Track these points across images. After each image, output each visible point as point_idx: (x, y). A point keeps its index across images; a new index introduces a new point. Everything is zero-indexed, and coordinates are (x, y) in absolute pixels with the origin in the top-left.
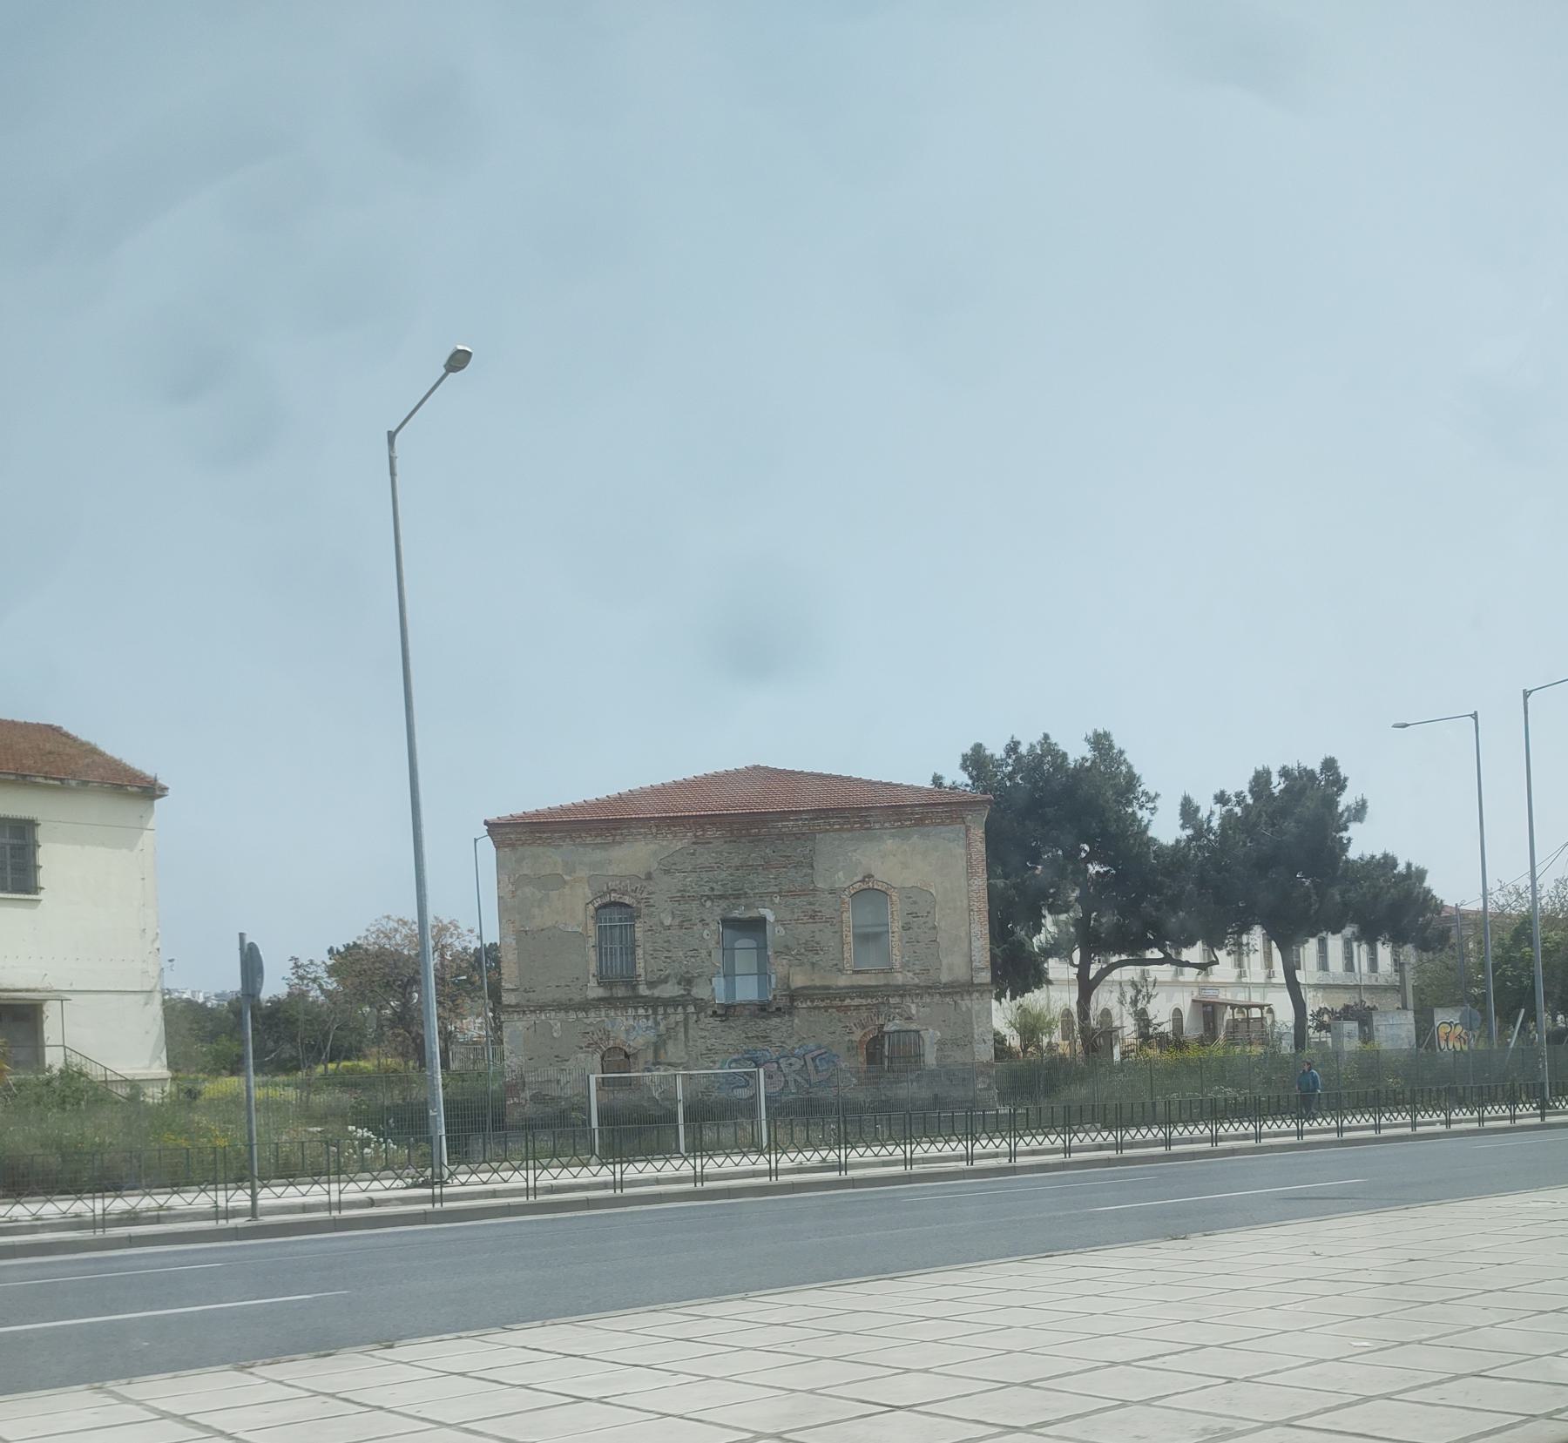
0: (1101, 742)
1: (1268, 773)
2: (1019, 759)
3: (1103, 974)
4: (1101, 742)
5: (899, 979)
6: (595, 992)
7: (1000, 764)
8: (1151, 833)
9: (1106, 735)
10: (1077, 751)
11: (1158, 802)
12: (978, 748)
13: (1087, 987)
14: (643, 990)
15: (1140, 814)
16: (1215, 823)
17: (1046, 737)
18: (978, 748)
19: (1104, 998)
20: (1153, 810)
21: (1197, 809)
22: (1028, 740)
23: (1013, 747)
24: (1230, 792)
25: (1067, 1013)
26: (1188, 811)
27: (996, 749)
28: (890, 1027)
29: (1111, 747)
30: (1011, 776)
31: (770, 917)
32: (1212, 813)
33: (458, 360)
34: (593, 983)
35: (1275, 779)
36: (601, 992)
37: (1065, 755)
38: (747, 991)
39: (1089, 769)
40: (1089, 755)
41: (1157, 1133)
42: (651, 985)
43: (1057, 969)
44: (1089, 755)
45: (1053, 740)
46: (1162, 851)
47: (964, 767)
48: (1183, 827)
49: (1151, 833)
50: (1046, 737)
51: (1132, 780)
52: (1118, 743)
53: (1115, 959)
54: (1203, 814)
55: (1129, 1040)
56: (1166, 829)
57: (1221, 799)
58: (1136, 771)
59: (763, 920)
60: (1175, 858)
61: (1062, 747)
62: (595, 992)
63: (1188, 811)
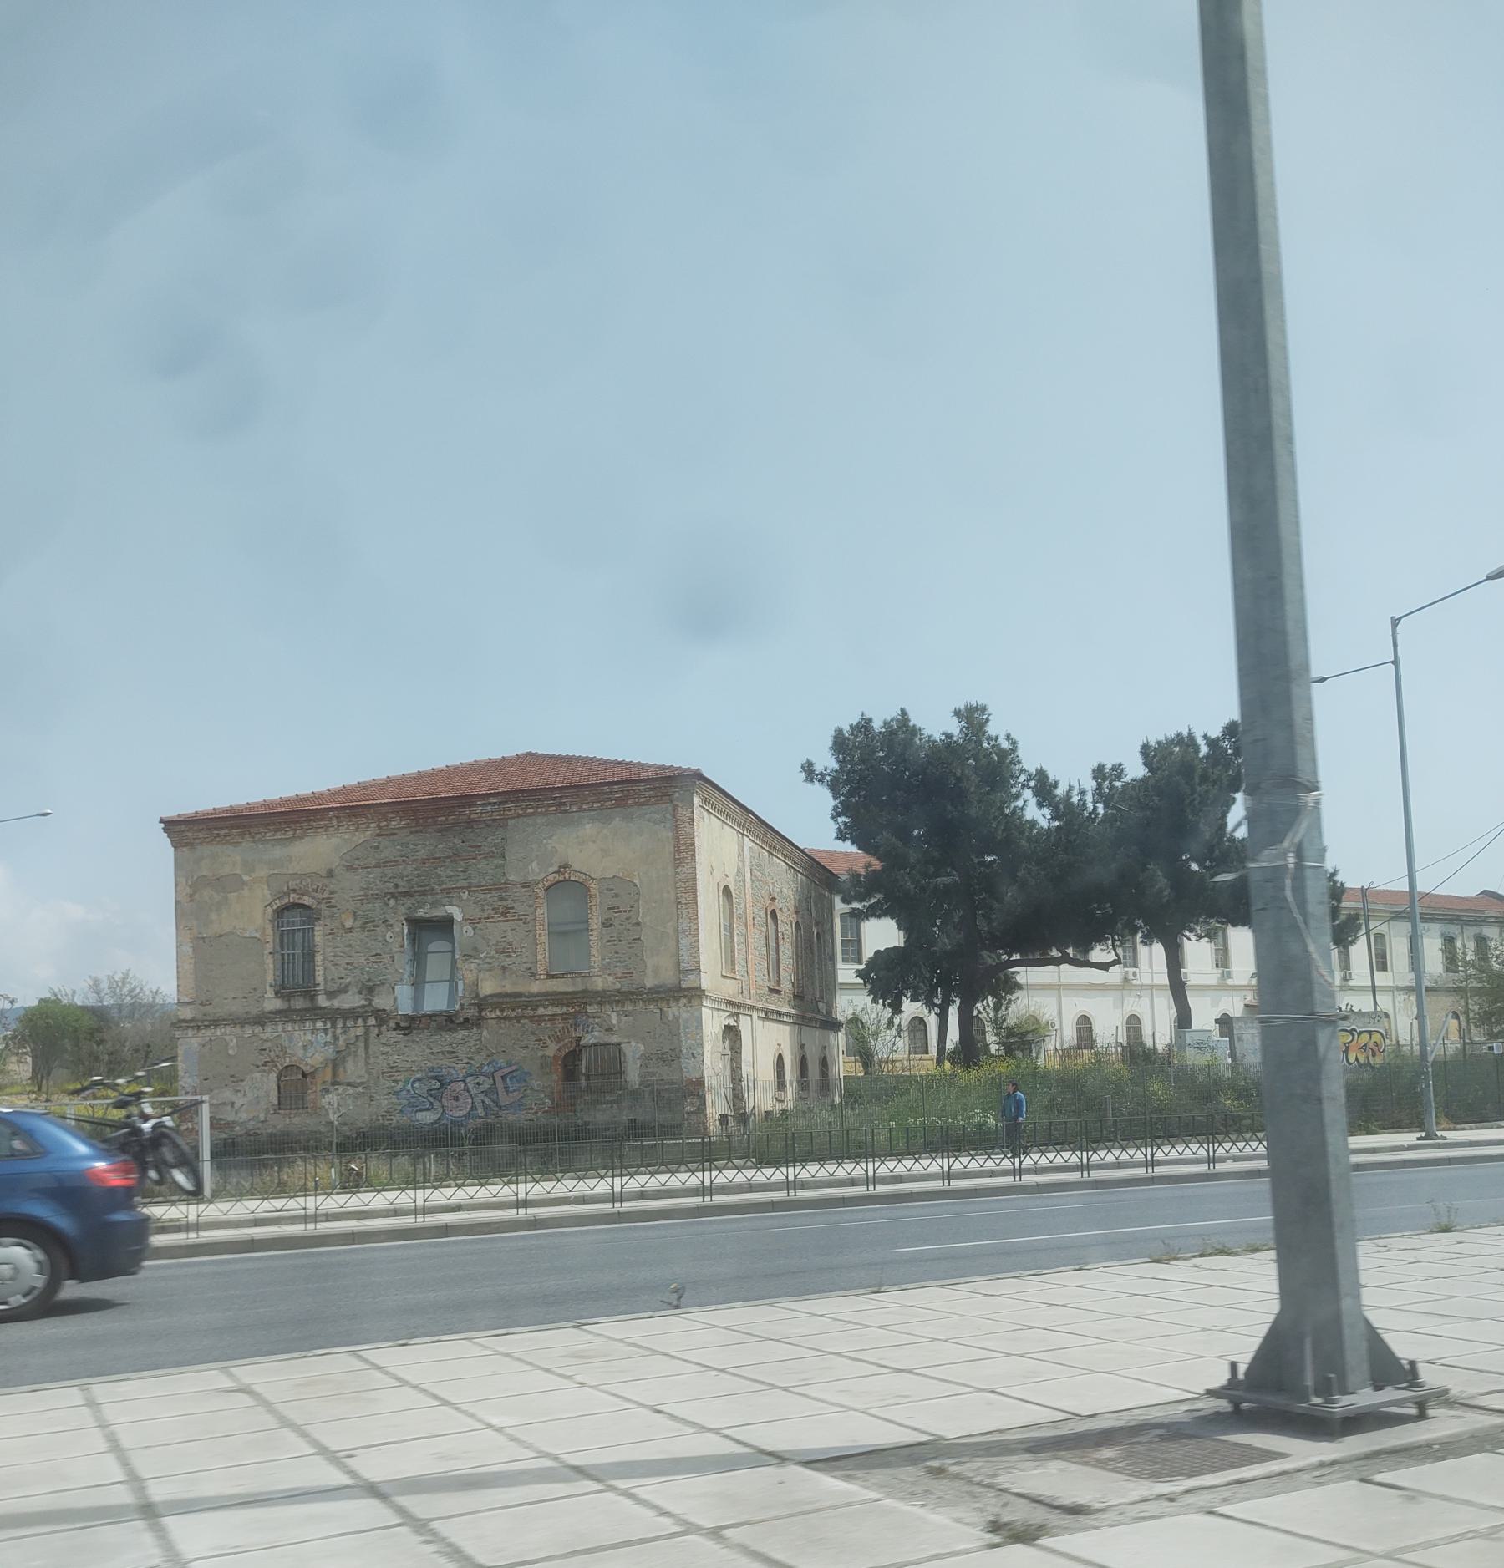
4: (973, 717)
5: (599, 984)
6: (272, 1003)
14: (322, 1001)
31: (458, 916)
34: (270, 994)
42: (331, 995)
48: (835, 798)
50: (903, 712)
62: (272, 1003)
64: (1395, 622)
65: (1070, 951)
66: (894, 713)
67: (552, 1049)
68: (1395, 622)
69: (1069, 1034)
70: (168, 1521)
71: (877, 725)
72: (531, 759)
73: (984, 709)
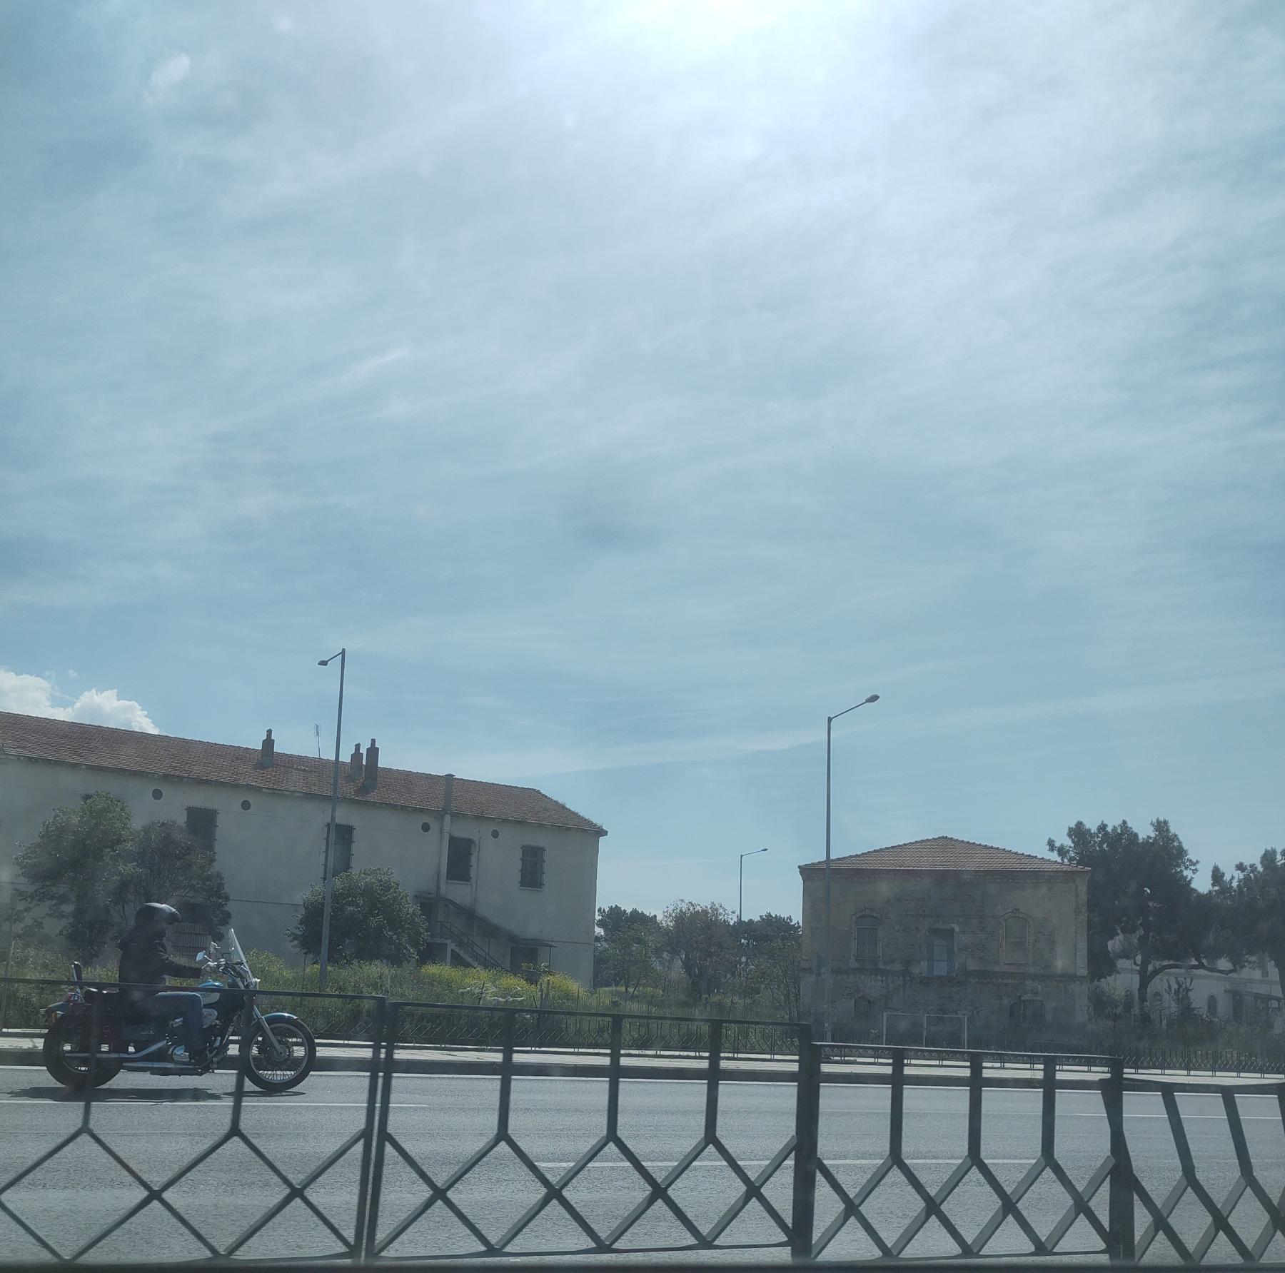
0: (1161, 826)
1: (1274, 852)
2: (1107, 833)
3: (1156, 972)
4: (1161, 826)
5: (1031, 970)
6: (853, 964)
7: (1092, 836)
8: (1193, 886)
9: (1166, 823)
10: (1144, 831)
11: (1198, 866)
12: (1079, 824)
13: (1145, 980)
14: (881, 966)
15: (1185, 873)
16: (1235, 884)
17: (1124, 822)
18: (1079, 824)
19: (1158, 984)
20: (1195, 871)
21: (1223, 875)
22: (1113, 823)
23: (1103, 827)
24: (1247, 863)
25: (1129, 996)
26: (1217, 876)
27: (1092, 825)
28: (1025, 997)
29: (1168, 830)
30: (1100, 845)
31: (957, 929)
32: (1233, 878)
33: (874, 698)
34: (853, 959)
35: (1279, 857)
36: (856, 965)
37: (1136, 835)
38: (941, 969)
39: (1152, 844)
40: (1153, 835)
41: (1159, 1071)
42: (885, 963)
43: (1122, 963)
44: (1153, 835)
45: (1129, 825)
46: (1200, 896)
47: (1069, 835)
48: (1213, 885)
49: (1193, 886)
50: (1124, 822)
51: (1181, 852)
52: (1173, 830)
53: (1166, 963)
54: (1227, 877)
55: (1121, 937)
56: (1202, 883)
57: (1240, 867)
58: (1185, 846)
59: (953, 930)
60: (1205, 899)
61: (1135, 830)
62: (853, 964)
63: (1217, 876)
64: (830, 720)
65: (1204, 961)
66: (1118, 822)
67: (1005, 1001)
68: (830, 720)
69: (1173, 1007)
70: (1010, 1218)
71: (1109, 829)
72: (945, 843)
73: (1166, 823)
